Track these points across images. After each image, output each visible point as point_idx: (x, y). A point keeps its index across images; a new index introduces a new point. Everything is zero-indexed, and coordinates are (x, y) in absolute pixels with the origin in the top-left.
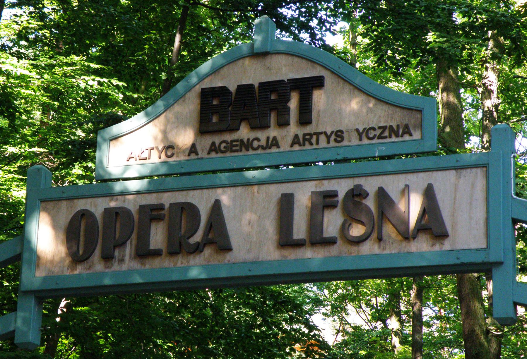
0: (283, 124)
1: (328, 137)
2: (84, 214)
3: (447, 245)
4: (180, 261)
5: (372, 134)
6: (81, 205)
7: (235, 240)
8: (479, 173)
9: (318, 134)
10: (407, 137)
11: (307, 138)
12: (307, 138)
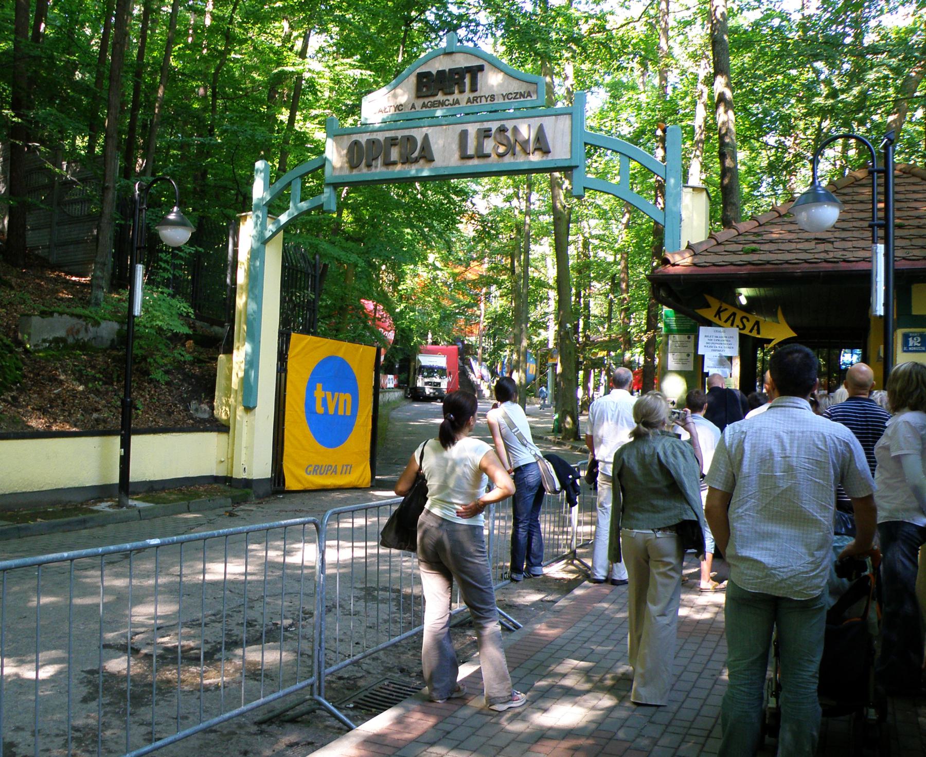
0: (462, 91)
1: (487, 99)
2: (356, 143)
3: (550, 157)
4: (406, 167)
5: (510, 96)
6: (355, 137)
7: (436, 157)
8: (568, 118)
9: (481, 97)
10: (529, 98)
11: (475, 99)
12: (475, 99)
